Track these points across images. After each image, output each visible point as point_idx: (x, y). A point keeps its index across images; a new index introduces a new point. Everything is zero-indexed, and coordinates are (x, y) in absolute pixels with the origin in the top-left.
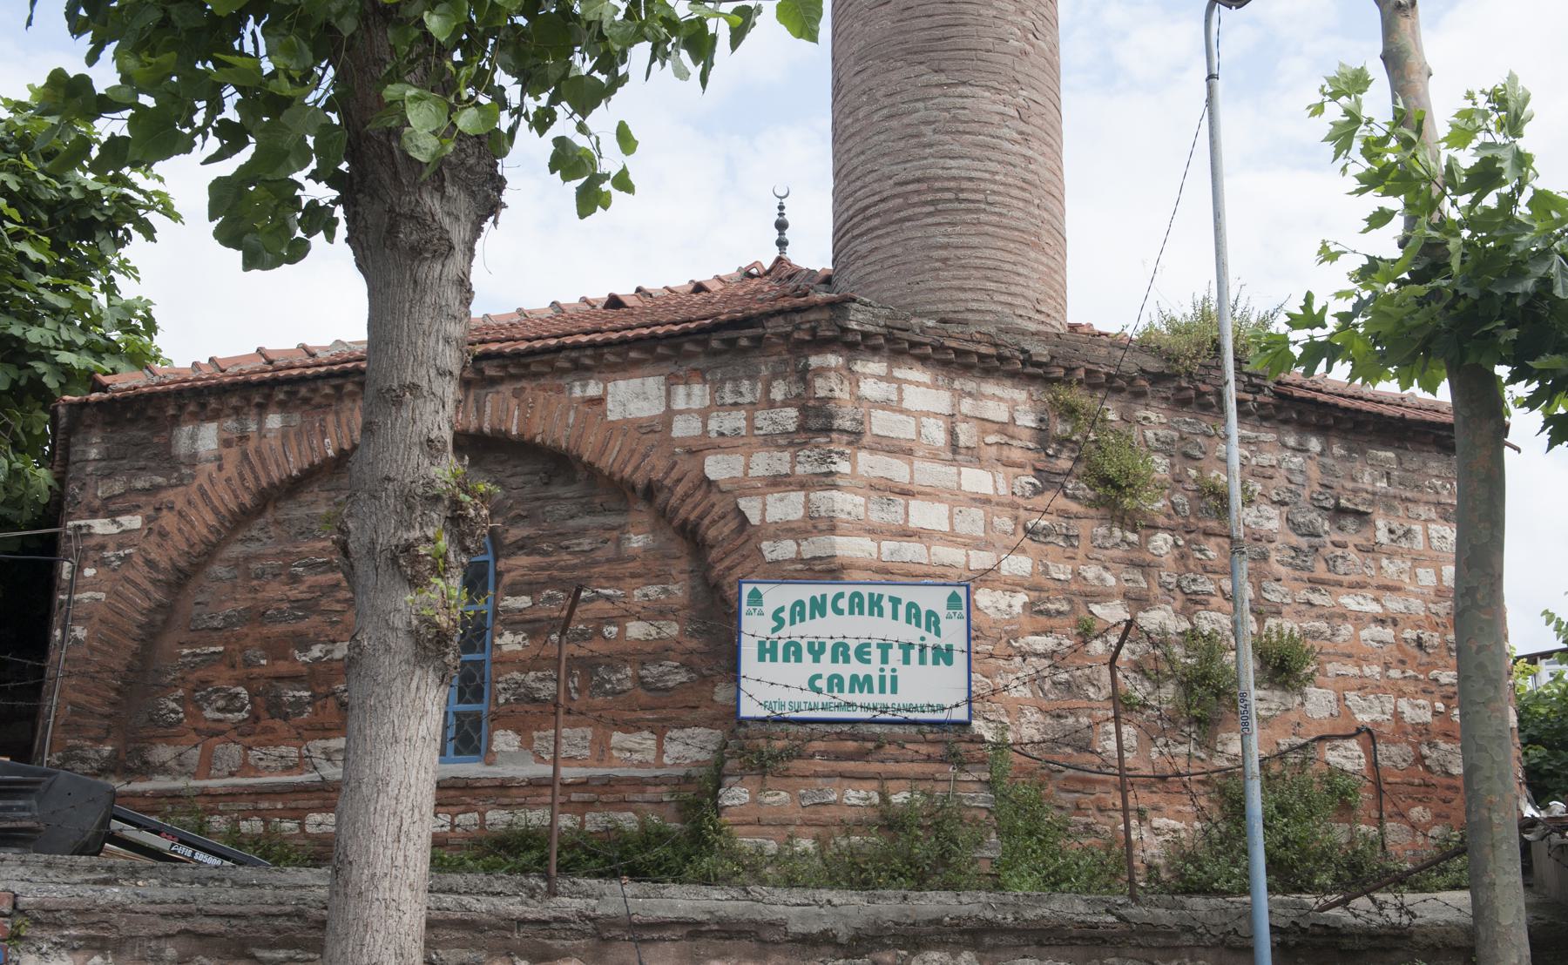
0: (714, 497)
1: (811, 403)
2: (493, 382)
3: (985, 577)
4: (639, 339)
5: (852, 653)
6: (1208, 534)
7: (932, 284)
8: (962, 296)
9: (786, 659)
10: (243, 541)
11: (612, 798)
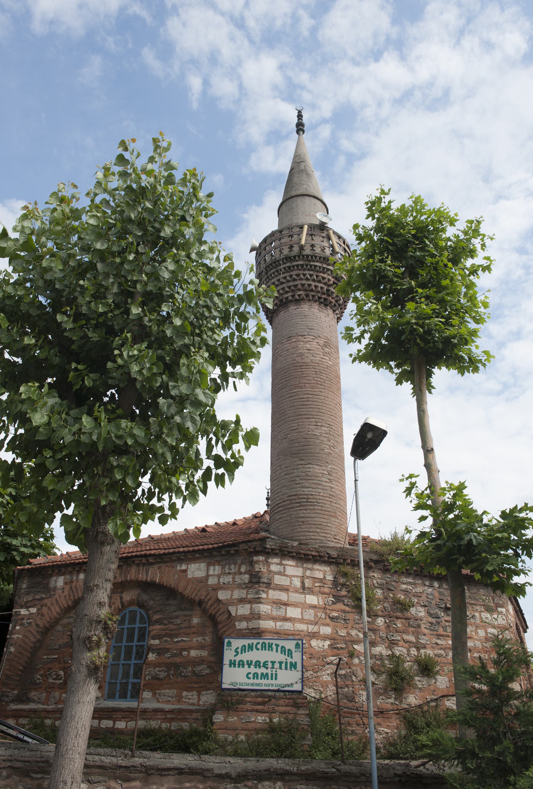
0: (221, 606)
1: (254, 573)
2: (152, 564)
3: (314, 635)
4: (199, 550)
5: (262, 665)
6: (397, 618)
7: (300, 530)
8: (309, 534)
9: (239, 667)
10: (68, 618)
11: (181, 717)
